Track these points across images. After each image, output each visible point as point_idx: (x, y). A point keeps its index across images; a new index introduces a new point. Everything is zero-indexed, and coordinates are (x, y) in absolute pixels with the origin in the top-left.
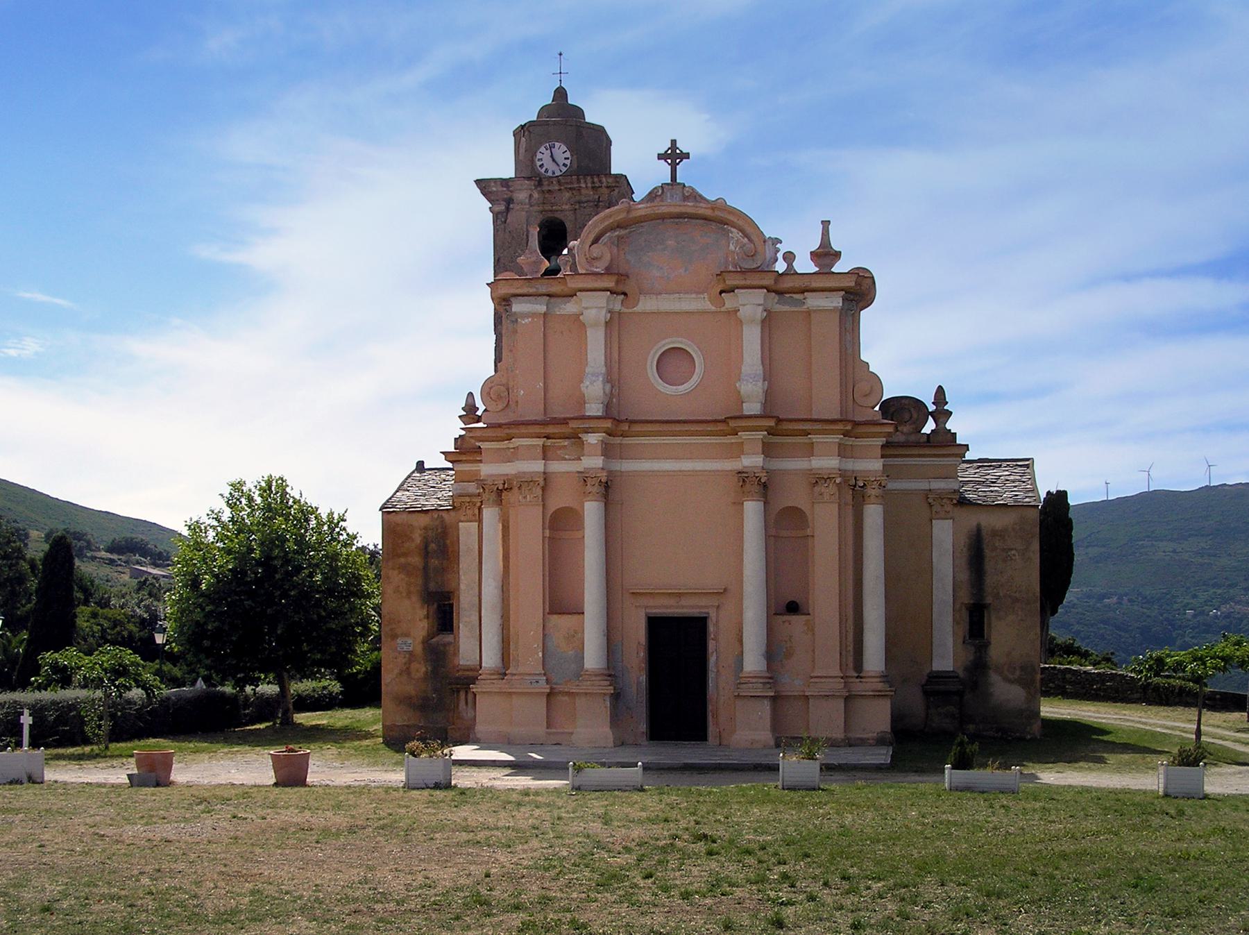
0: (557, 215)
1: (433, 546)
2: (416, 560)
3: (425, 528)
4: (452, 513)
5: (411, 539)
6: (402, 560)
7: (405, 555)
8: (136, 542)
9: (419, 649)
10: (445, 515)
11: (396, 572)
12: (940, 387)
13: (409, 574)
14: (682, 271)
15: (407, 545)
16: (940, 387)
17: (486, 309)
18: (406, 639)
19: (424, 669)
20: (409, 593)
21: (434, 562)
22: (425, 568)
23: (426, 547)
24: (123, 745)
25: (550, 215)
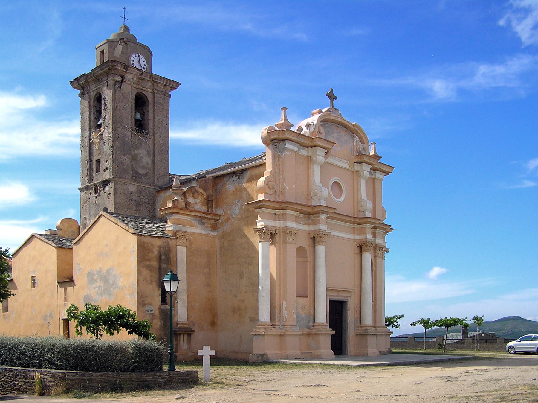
0: (144, 92)
1: (163, 257)
2: (155, 264)
3: (160, 247)
4: (173, 241)
5: (152, 251)
6: (148, 263)
7: (149, 260)
8: (58, 256)
9: (157, 312)
10: (169, 240)
11: (144, 269)
12: (178, 84)
13: (151, 271)
14: (339, 148)
15: (150, 254)
16: (178, 84)
17: (80, 123)
18: (150, 307)
19: (159, 323)
20: (151, 281)
21: (164, 266)
22: (160, 268)
23: (160, 256)
24: (189, 370)
25: (141, 91)
